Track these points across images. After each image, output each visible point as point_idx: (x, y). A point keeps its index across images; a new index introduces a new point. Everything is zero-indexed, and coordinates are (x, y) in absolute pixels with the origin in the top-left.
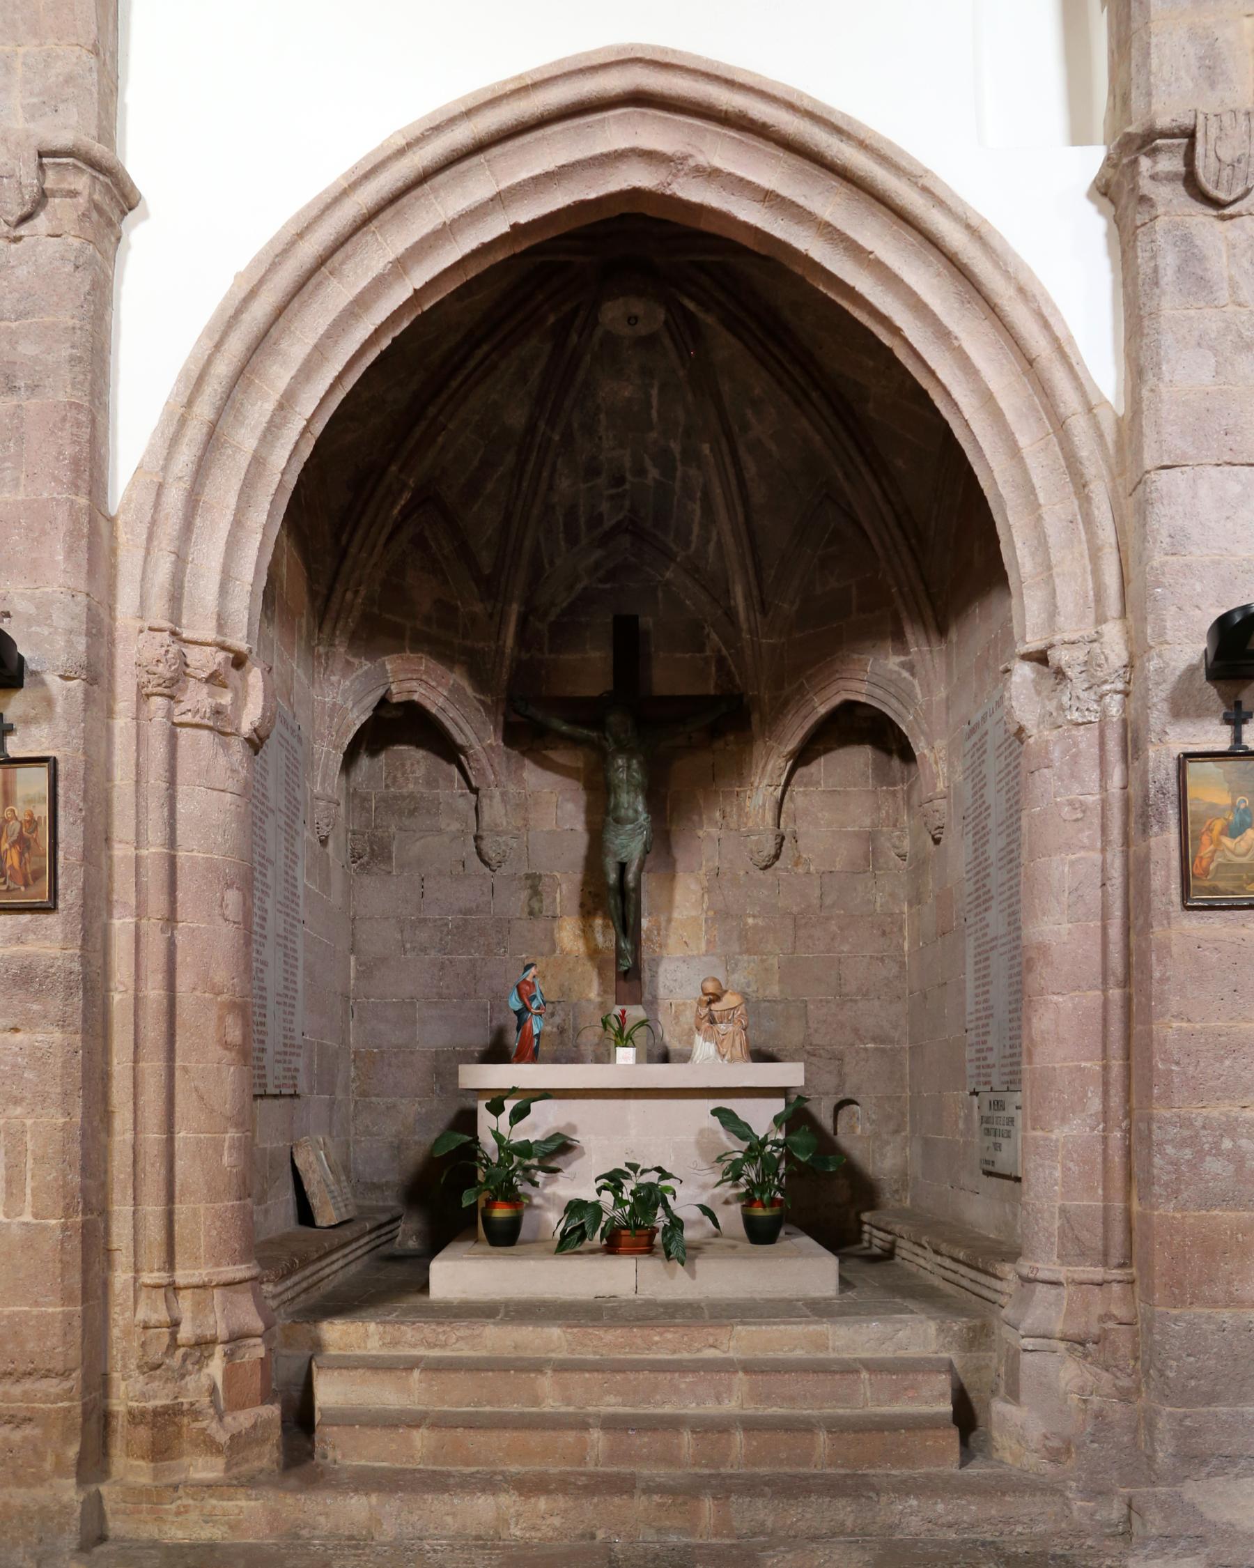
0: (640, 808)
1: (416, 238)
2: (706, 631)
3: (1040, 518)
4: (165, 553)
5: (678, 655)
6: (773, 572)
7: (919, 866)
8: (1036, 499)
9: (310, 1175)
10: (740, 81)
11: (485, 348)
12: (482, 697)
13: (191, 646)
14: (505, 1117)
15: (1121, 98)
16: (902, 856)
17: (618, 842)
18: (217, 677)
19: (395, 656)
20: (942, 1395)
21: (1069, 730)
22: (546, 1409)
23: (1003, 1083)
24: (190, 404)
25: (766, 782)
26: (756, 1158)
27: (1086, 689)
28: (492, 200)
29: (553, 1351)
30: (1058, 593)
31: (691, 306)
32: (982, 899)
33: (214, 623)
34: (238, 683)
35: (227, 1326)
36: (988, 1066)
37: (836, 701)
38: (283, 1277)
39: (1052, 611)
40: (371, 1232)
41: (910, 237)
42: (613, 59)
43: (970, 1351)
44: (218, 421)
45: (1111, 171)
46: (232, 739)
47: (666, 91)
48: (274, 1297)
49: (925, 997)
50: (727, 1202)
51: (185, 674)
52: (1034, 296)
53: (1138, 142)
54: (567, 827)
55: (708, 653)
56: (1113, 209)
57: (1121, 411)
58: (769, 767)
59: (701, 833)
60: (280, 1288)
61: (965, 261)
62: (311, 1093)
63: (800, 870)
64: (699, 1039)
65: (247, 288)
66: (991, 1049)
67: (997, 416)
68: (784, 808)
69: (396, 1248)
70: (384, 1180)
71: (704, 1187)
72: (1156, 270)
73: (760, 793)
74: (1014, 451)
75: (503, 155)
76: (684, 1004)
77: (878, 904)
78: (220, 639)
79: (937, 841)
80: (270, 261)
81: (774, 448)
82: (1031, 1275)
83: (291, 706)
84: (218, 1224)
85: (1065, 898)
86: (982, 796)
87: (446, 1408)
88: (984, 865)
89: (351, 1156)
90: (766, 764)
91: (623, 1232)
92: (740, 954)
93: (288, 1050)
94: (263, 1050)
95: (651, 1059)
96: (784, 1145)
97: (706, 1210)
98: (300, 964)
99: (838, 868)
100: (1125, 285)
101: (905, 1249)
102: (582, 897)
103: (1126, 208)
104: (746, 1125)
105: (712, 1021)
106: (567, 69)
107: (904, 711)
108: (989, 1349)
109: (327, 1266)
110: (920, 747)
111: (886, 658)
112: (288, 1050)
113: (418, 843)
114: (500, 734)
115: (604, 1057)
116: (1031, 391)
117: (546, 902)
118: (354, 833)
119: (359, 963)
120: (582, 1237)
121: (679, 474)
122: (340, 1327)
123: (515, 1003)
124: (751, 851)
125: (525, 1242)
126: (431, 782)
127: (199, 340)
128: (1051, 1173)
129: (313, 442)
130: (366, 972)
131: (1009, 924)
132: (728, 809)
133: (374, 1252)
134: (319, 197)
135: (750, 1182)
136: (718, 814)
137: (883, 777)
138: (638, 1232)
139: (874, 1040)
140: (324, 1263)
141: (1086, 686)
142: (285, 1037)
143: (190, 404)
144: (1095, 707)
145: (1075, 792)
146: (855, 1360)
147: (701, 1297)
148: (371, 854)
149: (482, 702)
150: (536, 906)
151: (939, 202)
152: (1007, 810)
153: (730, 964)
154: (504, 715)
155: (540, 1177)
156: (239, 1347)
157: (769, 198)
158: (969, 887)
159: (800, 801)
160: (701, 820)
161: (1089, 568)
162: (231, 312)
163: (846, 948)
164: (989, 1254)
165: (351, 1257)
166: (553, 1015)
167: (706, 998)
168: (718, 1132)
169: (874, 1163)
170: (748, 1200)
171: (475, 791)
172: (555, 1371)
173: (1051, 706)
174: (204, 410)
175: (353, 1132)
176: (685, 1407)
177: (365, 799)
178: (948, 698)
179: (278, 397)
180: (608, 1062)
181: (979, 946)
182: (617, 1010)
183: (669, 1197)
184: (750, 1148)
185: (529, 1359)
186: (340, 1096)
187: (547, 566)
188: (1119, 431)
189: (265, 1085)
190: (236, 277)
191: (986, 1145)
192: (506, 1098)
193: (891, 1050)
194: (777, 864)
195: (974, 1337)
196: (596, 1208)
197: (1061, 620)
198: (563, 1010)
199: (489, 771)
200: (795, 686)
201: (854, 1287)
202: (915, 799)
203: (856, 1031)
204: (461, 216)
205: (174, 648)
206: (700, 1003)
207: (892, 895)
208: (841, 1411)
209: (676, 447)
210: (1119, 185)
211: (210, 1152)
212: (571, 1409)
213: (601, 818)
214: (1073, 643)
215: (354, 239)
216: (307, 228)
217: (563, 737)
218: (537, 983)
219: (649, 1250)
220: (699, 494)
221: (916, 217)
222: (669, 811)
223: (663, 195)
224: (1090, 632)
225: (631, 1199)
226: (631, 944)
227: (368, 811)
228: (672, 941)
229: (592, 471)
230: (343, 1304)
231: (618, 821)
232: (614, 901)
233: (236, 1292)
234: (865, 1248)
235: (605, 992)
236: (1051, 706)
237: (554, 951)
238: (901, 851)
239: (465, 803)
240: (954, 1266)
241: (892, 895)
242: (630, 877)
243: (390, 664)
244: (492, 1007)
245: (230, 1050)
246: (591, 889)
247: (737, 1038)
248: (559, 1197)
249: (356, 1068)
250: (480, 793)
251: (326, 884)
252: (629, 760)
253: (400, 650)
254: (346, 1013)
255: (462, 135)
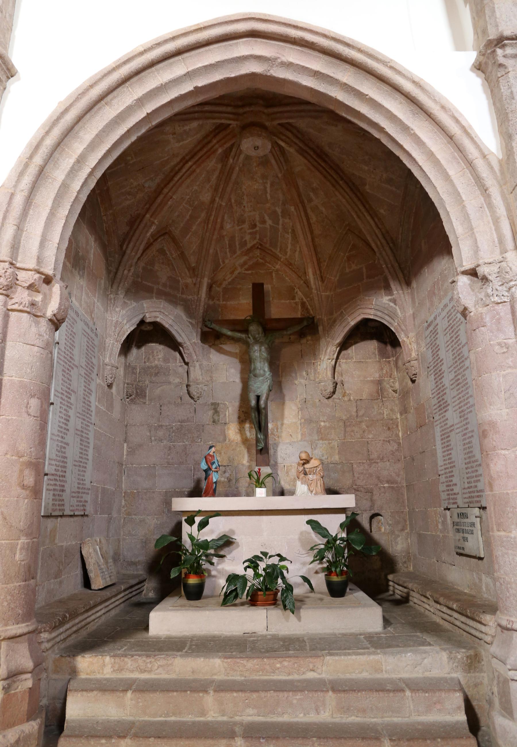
0: (266, 369)
1: (148, 90)
2: (296, 291)
3: (464, 207)
4: (11, 225)
5: (283, 301)
6: (326, 264)
7: (404, 395)
8: (461, 198)
9: (90, 560)
10: (301, 26)
11: (190, 163)
12: (191, 321)
13: (21, 271)
14: (195, 526)
15: (480, 30)
16: (395, 391)
17: (255, 386)
18: (34, 287)
19: (148, 300)
20: (459, 708)
21: (493, 307)
22: (210, 719)
23: (465, 503)
24: (31, 157)
25: (327, 357)
26: (331, 548)
27: (500, 285)
28: (185, 75)
29: (215, 674)
30: (478, 240)
31: (282, 144)
32: (443, 406)
33: (35, 260)
34: (47, 292)
35: (7, 668)
36: (455, 494)
37: (359, 319)
38: (54, 628)
39: (476, 250)
40: (125, 590)
41: (386, 88)
42: (241, 18)
43: (469, 672)
44: (45, 167)
45: (482, 57)
46: (41, 319)
47: (266, 30)
48: (48, 641)
49: (413, 460)
50: (317, 572)
51: (16, 284)
52: (450, 109)
53: (495, 42)
54: (232, 380)
55: (297, 300)
56: (483, 75)
57: (501, 157)
58: (328, 351)
59: (296, 382)
60: (54, 634)
61: (414, 95)
62: (96, 514)
63: (346, 399)
64: (299, 483)
65: (63, 108)
66: (456, 485)
67: (436, 163)
68: (336, 370)
69: (142, 598)
70: (137, 560)
71: (304, 564)
72: (512, 93)
73: (324, 362)
74: (447, 177)
75: (190, 56)
76: (291, 466)
77: (385, 415)
78: (36, 268)
79: (413, 381)
80: (76, 96)
81: (324, 209)
82: (509, 626)
83: (93, 319)
84: (9, 598)
85: (502, 395)
86: (438, 355)
87: (147, 718)
88: (442, 389)
89: (109, 551)
90: (326, 349)
91: (260, 593)
92: (318, 440)
93: (81, 491)
94: (63, 491)
95: (274, 494)
96: (347, 541)
97: (306, 580)
98: (91, 446)
99: (364, 397)
100: (494, 104)
101: (415, 598)
102: (239, 413)
103: (491, 72)
104: (325, 529)
105: (305, 474)
106: (219, 21)
107: (392, 321)
108: (481, 671)
109: (93, 614)
110: (401, 337)
111: (382, 298)
112: (81, 491)
113: (159, 389)
114: (199, 337)
115: (250, 494)
116: (453, 150)
117: (221, 416)
118: (128, 384)
119: (129, 448)
120: (236, 597)
121: (281, 222)
122: (88, 659)
123: (204, 466)
124: (321, 390)
125: (207, 597)
126: (166, 360)
127: (38, 129)
128: (513, 559)
129: (96, 181)
130: (132, 452)
131: (460, 417)
132: (309, 371)
133: (128, 601)
134: (101, 71)
135: (328, 561)
136: (304, 373)
137: (383, 354)
138: (267, 593)
139: (388, 482)
140: (90, 613)
141: (501, 283)
142: (79, 484)
143: (31, 157)
144: (507, 294)
145: (501, 338)
146: (400, 679)
147: (305, 632)
148: (136, 394)
149: (191, 323)
150: (216, 418)
151: (399, 72)
152: (453, 359)
153: (313, 445)
154: (201, 329)
155: (215, 560)
156: (14, 682)
157: (316, 74)
158: (435, 401)
159: (344, 366)
160: (296, 376)
161: (493, 228)
162: (55, 118)
163: (371, 436)
164: (474, 607)
165: (111, 606)
166: (225, 472)
167: (302, 462)
168: (310, 533)
169: (392, 547)
170: (328, 571)
171: (187, 364)
172: (215, 691)
173: (482, 295)
174: (38, 160)
175: (122, 533)
176: (297, 716)
177: (134, 368)
178: (414, 314)
179: (77, 157)
180: (253, 496)
181: (443, 430)
182: (256, 469)
183: (285, 572)
184: (328, 542)
185: (201, 680)
186: (115, 515)
187: (221, 263)
188: (501, 165)
189: (64, 510)
190: (59, 103)
191: (457, 538)
192: (195, 516)
193: (397, 487)
194: (334, 396)
195: (471, 663)
196: (244, 579)
197: (481, 253)
198: (230, 469)
199: (194, 355)
200: (339, 313)
201: (391, 624)
202: (400, 363)
203: (378, 478)
204: (170, 82)
205: (10, 271)
206: (299, 464)
207: (392, 410)
208: (395, 720)
209: (279, 211)
210: (486, 63)
211: (8, 552)
212: (225, 719)
213: (247, 372)
214: (490, 264)
215: (118, 90)
216: (95, 83)
217: (229, 338)
218: (215, 456)
219: (274, 603)
220: (290, 230)
221: (388, 79)
222: (280, 371)
223: (266, 76)
224: (499, 258)
225: (264, 574)
226: (264, 435)
227: (135, 374)
228: (284, 434)
229: (241, 221)
230: (93, 643)
231: (255, 376)
232: (255, 415)
233: (17, 643)
234: (391, 595)
235: (251, 460)
236: (482, 295)
237: (225, 440)
238: (394, 389)
239: (182, 370)
240: (449, 612)
241: (392, 410)
242: (262, 402)
243: (146, 304)
244: (194, 469)
245: (26, 490)
246: (244, 410)
247: (319, 482)
248: (226, 571)
249: (125, 500)
250: (189, 365)
251: (110, 406)
252: (260, 347)
253: (152, 298)
254: (121, 472)
255: (170, 47)
